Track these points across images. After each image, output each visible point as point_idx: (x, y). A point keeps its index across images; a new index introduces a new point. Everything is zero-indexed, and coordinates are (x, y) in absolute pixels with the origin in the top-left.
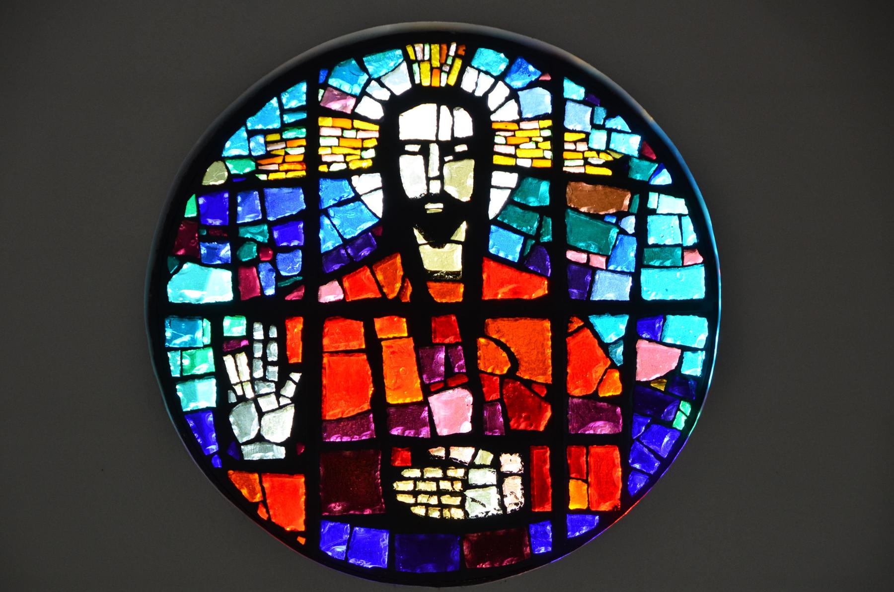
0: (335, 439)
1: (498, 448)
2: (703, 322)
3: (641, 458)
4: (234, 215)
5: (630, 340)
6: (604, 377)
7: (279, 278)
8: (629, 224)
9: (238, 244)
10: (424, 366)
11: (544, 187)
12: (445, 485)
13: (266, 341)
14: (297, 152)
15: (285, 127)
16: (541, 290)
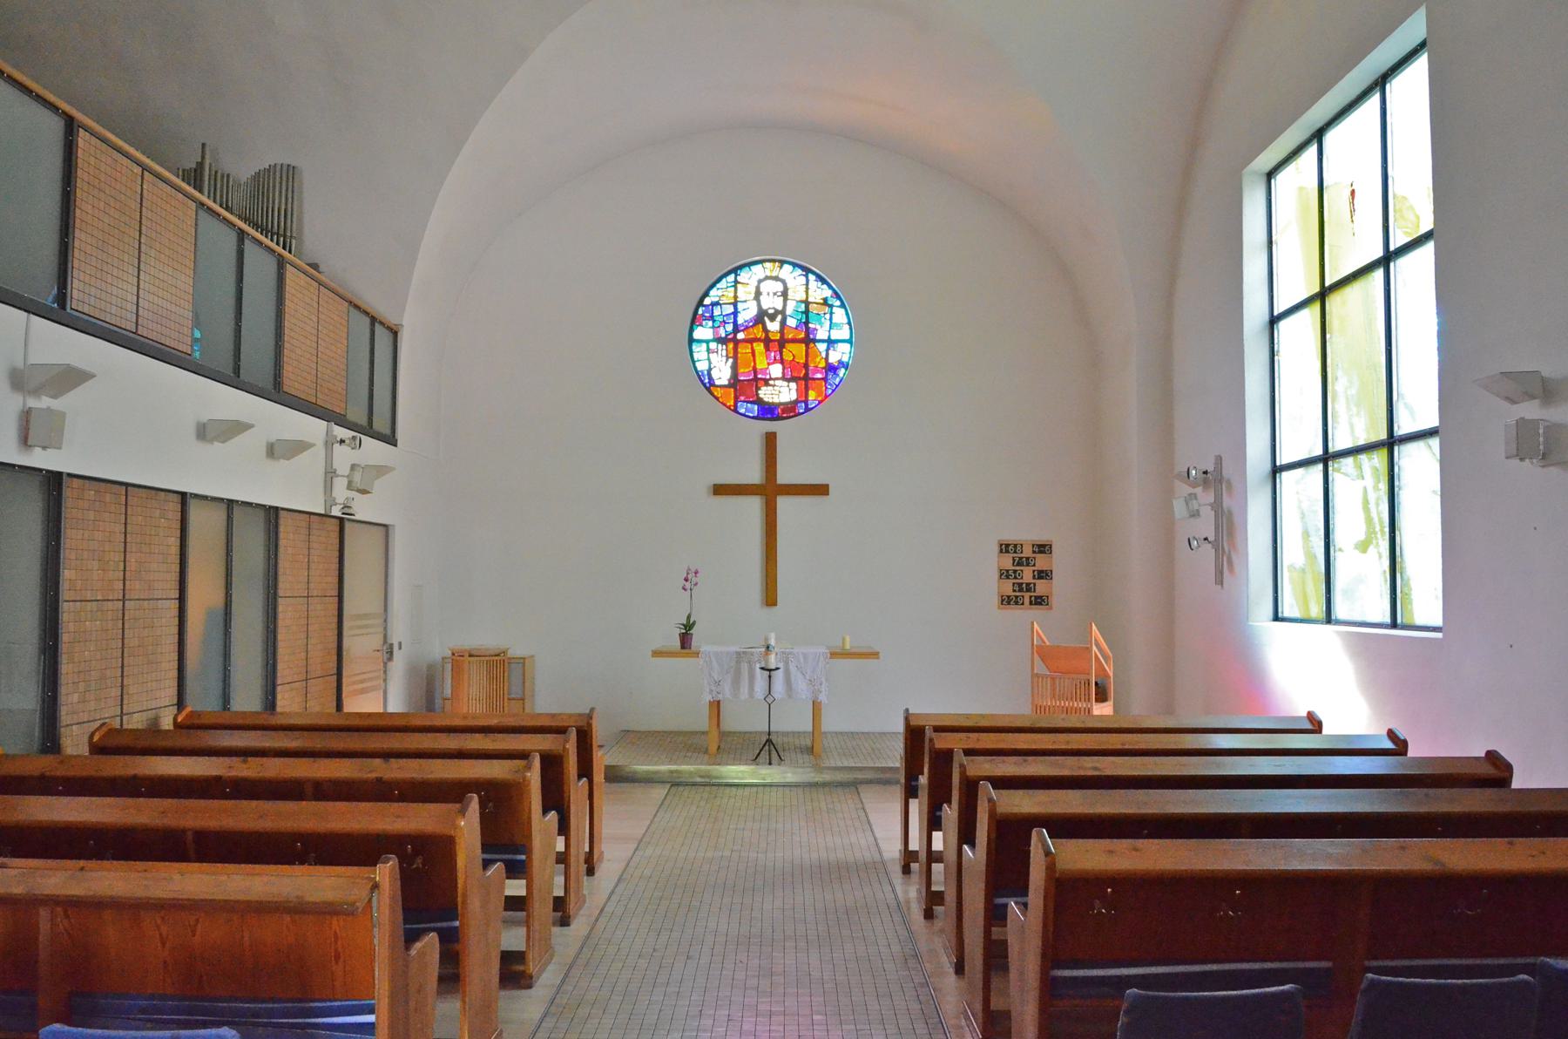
0: (742, 378)
1: (789, 380)
2: (849, 345)
3: (830, 384)
4: (713, 313)
5: (827, 350)
6: (804, 372)
7: (726, 331)
8: (828, 316)
9: (714, 321)
10: (768, 357)
11: (803, 305)
12: (773, 392)
13: (722, 350)
14: (732, 295)
15: (727, 287)
16: (802, 335)
